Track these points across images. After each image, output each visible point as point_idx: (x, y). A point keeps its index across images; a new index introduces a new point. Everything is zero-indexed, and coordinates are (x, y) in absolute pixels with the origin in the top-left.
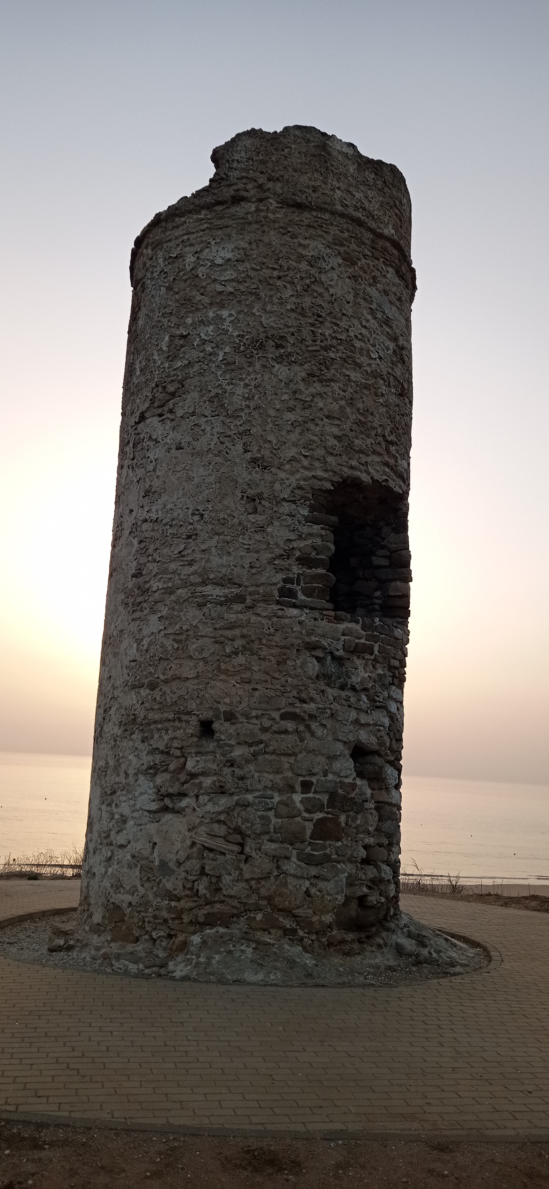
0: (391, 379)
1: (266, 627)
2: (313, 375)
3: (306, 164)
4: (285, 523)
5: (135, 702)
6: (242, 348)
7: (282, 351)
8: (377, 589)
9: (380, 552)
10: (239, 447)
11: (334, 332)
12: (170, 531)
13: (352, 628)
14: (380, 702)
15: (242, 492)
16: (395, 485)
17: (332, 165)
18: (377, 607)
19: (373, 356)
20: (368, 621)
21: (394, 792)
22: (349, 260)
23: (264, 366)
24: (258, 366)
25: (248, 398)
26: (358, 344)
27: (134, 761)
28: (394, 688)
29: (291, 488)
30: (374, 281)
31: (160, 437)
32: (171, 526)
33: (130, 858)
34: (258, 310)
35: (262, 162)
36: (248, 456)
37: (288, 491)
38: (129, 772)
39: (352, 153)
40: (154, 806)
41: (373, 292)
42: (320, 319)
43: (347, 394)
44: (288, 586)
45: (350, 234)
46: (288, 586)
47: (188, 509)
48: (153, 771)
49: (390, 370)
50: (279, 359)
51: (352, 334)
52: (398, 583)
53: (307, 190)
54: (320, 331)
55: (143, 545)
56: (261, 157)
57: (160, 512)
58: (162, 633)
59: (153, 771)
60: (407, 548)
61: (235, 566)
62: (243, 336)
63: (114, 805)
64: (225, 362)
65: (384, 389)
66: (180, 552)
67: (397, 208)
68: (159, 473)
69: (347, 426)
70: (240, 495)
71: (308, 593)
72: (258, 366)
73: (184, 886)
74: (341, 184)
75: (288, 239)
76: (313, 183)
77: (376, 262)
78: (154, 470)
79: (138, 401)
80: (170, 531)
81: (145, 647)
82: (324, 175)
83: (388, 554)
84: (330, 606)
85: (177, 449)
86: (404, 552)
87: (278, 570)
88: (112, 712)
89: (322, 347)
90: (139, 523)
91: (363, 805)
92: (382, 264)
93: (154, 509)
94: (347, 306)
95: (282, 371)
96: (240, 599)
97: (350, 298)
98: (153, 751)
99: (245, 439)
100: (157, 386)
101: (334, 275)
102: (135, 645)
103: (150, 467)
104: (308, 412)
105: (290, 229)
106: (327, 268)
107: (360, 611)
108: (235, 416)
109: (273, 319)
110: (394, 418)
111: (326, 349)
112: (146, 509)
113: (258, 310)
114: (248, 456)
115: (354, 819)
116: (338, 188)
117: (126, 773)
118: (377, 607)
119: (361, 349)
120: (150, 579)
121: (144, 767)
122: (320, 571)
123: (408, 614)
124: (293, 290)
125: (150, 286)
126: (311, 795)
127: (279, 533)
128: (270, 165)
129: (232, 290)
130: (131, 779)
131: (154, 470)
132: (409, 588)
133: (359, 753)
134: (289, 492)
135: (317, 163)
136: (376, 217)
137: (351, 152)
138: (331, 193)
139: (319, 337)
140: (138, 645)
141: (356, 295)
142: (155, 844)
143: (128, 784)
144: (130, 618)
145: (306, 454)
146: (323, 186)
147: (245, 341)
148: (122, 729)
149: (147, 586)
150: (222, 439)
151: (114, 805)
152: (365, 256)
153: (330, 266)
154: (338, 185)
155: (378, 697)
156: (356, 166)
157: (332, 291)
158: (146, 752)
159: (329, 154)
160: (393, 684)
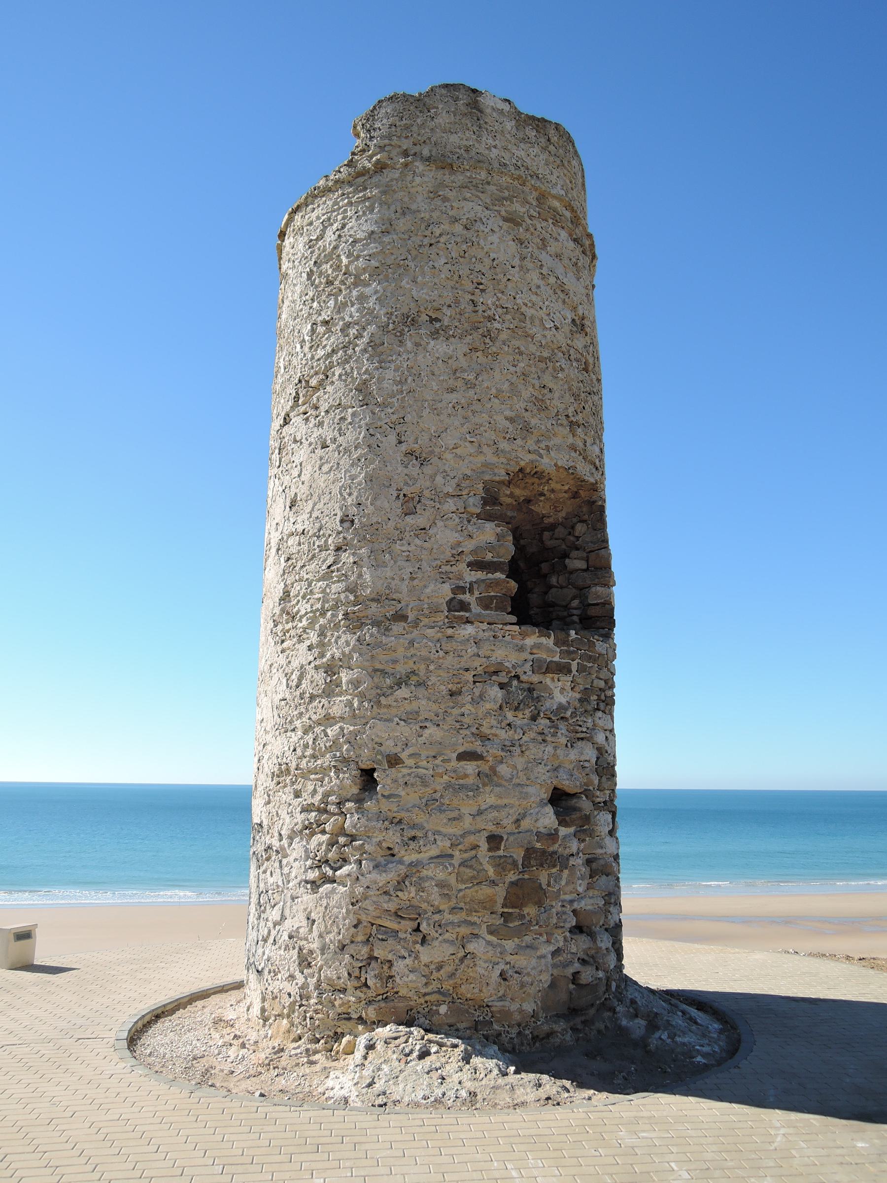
0: (572, 352)
1: (434, 651)
2: (476, 350)
3: (456, 123)
4: (450, 523)
5: (286, 749)
6: (391, 326)
7: (438, 325)
8: (574, 598)
9: (574, 554)
10: (392, 438)
11: (498, 299)
12: (317, 543)
13: (541, 644)
14: (582, 732)
15: (397, 490)
16: (584, 470)
17: (486, 123)
18: (575, 618)
19: (548, 326)
20: (561, 635)
21: (608, 841)
22: (512, 220)
23: (417, 345)
24: (409, 344)
25: (400, 382)
26: (529, 312)
27: (288, 819)
28: (599, 714)
29: (456, 480)
30: (543, 244)
31: (304, 437)
32: (318, 537)
33: (287, 938)
34: (408, 283)
35: (407, 127)
36: (404, 447)
37: (453, 483)
38: (283, 833)
39: (508, 109)
40: (313, 875)
41: (544, 256)
42: (481, 287)
43: (518, 369)
44: (461, 597)
45: (511, 193)
46: (461, 597)
47: (336, 515)
48: (310, 829)
49: (569, 342)
50: (435, 335)
51: (519, 301)
52: (598, 588)
53: (458, 150)
54: (481, 300)
55: (290, 562)
56: (404, 122)
57: (307, 523)
58: (312, 665)
59: (310, 829)
60: (606, 548)
61: (393, 579)
62: (391, 314)
63: (268, 873)
64: (372, 344)
65: (563, 363)
66: (329, 567)
67: (566, 168)
68: (303, 478)
69: (520, 405)
70: (395, 494)
71: (485, 603)
72: (409, 344)
73: (349, 974)
74: (497, 142)
75: (439, 203)
76: (465, 143)
77: (544, 224)
78: (299, 476)
79: (282, 401)
80: (317, 543)
81: (294, 684)
82: (477, 133)
83: (585, 555)
84: (514, 619)
85: (322, 448)
86: (603, 552)
87: (444, 578)
88: (264, 761)
89: (484, 317)
90: (285, 538)
91: (568, 859)
92: (551, 225)
93: (300, 519)
94: (512, 271)
95: (439, 347)
96: (400, 617)
97: (516, 262)
98: (305, 810)
99: (399, 428)
100: (300, 381)
101: (494, 238)
102: (284, 681)
103: (295, 473)
104: (471, 393)
105: (440, 193)
106: (486, 230)
107: (555, 623)
108: (384, 405)
109: (425, 291)
110: (579, 396)
111: (491, 319)
112: (292, 520)
113: (408, 283)
114: (404, 447)
115: (558, 879)
116: (495, 147)
117: (280, 835)
118: (575, 618)
119: (532, 318)
120: (298, 601)
121: (299, 827)
122: (499, 575)
123: (612, 623)
124: (447, 258)
125: (292, 275)
126: (501, 853)
127: (445, 536)
128: (415, 128)
129: (377, 265)
130: (285, 842)
131: (299, 476)
132: (610, 595)
133: (559, 799)
134: (455, 486)
135: (468, 122)
136: (540, 176)
137: (506, 107)
138: (487, 152)
139: (480, 308)
140: (288, 680)
141: (523, 259)
142: (314, 921)
143: (282, 848)
144: (279, 648)
145: (472, 440)
146: (477, 145)
147: (394, 317)
148: (275, 781)
149: (295, 610)
150: (371, 431)
151: (268, 873)
152: (531, 217)
153: (489, 228)
154: (494, 144)
155: (580, 726)
156: (514, 122)
157: (493, 255)
158: (299, 809)
159: (481, 111)
160: (598, 709)
